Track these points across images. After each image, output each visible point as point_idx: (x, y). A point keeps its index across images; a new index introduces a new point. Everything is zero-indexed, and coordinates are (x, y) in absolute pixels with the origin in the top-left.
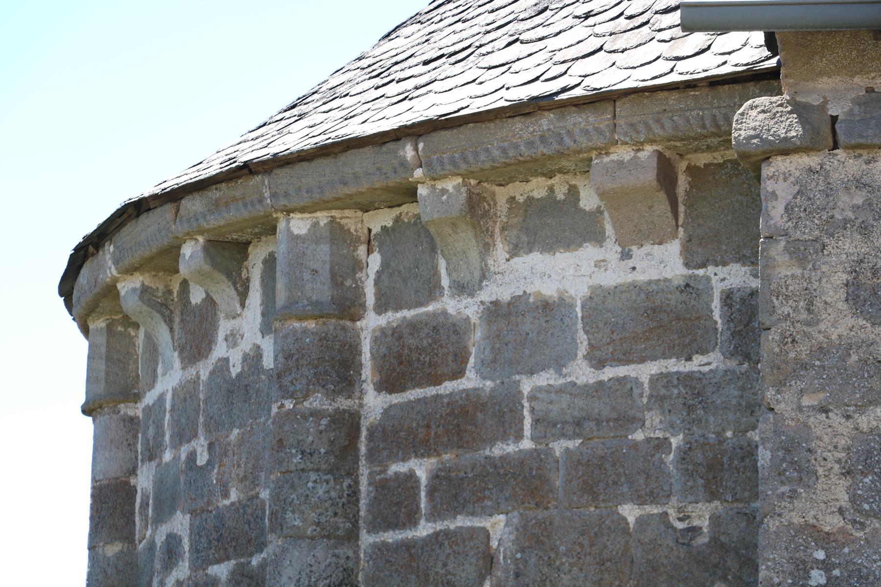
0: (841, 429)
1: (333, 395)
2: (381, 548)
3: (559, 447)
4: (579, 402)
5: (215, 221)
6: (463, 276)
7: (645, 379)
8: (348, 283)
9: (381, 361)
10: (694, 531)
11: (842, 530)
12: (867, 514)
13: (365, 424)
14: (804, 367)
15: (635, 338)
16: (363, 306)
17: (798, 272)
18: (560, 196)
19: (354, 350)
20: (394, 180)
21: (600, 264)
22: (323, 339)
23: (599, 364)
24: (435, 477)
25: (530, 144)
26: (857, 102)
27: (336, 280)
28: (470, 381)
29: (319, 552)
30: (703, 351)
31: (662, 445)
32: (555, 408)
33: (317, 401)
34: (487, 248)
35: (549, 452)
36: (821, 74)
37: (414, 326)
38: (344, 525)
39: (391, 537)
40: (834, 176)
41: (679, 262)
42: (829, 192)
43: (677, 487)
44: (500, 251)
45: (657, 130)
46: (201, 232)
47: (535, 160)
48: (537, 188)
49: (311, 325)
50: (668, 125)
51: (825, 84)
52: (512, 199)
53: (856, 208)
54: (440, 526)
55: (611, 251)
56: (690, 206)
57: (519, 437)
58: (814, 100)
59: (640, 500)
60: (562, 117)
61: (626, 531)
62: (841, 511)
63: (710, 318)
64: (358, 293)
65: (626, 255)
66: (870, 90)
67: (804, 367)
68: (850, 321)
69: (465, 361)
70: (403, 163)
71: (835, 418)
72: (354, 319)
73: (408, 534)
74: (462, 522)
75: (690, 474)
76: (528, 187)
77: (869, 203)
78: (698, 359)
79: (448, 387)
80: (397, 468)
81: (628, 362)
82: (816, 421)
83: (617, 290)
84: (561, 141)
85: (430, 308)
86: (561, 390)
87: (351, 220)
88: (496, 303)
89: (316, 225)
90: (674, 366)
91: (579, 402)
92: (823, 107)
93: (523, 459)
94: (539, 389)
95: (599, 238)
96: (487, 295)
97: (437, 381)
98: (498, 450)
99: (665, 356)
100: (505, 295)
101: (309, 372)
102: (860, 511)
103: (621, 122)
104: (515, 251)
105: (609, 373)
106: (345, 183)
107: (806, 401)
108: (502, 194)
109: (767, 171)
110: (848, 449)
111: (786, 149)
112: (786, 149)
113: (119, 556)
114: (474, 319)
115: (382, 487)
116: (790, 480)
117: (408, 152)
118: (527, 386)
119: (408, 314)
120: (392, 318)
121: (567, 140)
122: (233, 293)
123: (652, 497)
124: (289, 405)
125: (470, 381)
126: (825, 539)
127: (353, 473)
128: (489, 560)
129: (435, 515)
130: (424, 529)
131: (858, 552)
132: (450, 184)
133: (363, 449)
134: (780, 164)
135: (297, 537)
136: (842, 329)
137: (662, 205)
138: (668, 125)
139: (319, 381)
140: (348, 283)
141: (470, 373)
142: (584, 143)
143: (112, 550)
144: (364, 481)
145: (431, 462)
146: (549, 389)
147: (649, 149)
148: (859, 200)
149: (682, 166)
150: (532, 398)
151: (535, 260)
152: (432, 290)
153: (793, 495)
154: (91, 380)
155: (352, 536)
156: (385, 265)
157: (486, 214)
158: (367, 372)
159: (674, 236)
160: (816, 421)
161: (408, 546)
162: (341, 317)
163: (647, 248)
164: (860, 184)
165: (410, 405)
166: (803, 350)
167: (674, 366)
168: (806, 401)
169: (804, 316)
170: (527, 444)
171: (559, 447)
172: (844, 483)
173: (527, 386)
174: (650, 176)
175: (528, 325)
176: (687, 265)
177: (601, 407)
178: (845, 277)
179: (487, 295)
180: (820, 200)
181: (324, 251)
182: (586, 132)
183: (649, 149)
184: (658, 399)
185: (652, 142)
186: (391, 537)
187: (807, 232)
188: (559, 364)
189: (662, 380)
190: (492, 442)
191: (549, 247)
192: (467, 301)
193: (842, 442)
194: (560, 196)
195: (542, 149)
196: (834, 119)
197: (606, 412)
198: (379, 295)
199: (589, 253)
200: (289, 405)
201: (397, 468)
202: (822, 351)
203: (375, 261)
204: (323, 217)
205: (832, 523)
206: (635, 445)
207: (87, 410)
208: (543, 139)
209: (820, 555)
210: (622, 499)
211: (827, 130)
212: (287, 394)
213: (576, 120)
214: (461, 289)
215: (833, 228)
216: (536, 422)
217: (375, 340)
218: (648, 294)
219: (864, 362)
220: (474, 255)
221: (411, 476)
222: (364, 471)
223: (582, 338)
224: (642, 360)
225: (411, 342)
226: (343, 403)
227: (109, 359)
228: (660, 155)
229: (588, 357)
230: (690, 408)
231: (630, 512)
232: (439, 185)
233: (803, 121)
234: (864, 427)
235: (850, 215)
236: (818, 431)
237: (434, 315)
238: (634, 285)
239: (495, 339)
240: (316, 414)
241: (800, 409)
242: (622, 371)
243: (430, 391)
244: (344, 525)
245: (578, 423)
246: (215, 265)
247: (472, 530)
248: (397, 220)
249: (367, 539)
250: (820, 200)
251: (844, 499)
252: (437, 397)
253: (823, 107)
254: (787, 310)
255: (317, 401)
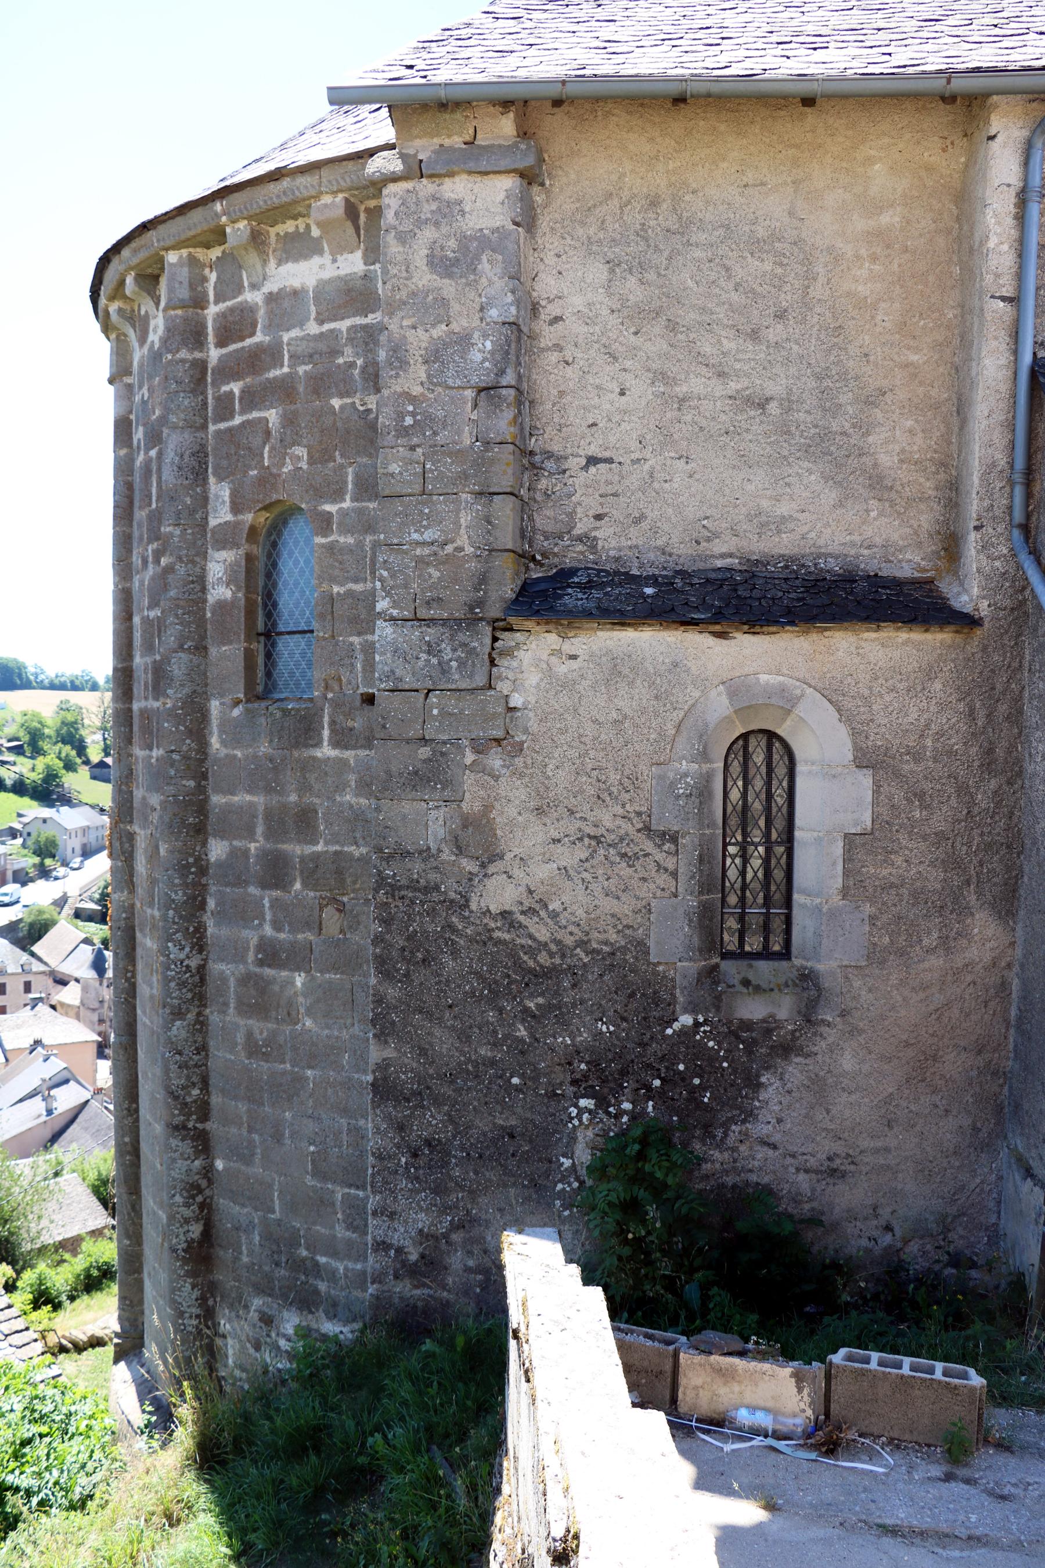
0: (423, 338)
1: (191, 350)
2: (218, 432)
3: (301, 370)
4: (312, 345)
5: (135, 261)
6: (254, 279)
7: (344, 329)
8: (199, 289)
9: (217, 331)
10: (369, 411)
11: (422, 394)
12: (435, 385)
13: (210, 366)
14: (404, 303)
15: (339, 307)
16: (208, 302)
17: (401, 249)
18: (302, 230)
19: (204, 327)
20: (213, 224)
21: (322, 267)
22: (186, 320)
23: (321, 322)
24: (243, 391)
25: (278, 196)
26: (434, 152)
27: (192, 287)
28: (259, 337)
29: (186, 436)
30: (373, 312)
31: (352, 365)
32: (300, 349)
33: (183, 354)
34: (265, 262)
35: (297, 373)
36: (416, 137)
37: (232, 310)
38: (199, 421)
39: (223, 426)
40: (421, 194)
41: (361, 262)
42: (417, 203)
43: (360, 387)
44: (272, 263)
45: (343, 183)
46: (132, 269)
47: (282, 206)
48: (289, 226)
49: (179, 312)
50: (348, 180)
51: (418, 143)
52: (278, 234)
53: (433, 212)
54: (245, 418)
55: (327, 258)
56: (366, 231)
57: (282, 366)
58: (411, 152)
59: (341, 396)
60: (294, 180)
61: (334, 413)
62: (422, 383)
63: (377, 293)
64: (205, 294)
65: (334, 261)
66: (441, 146)
67: (404, 303)
68: (429, 277)
69: (256, 327)
70: (216, 214)
71: (420, 332)
72: (203, 308)
73: (230, 424)
74: (255, 414)
75: (366, 380)
76: (285, 226)
77: (439, 209)
78: (371, 316)
79: (248, 342)
80: (225, 388)
81: (336, 320)
82: (410, 334)
83: (330, 281)
84: (293, 194)
85: (239, 299)
86: (302, 339)
87: (200, 253)
88: (270, 293)
89: (181, 257)
90: (359, 321)
91: (312, 345)
92: (415, 155)
93: (284, 378)
94: (292, 339)
95: (320, 252)
96: (266, 289)
97: (242, 339)
98: (274, 373)
99: (354, 316)
100: (275, 290)
101: (178, 338)
102: (432, 383)
103: (324, 180)
104: (279, 264)
105: (327, 327)
106: (190, 229)
107: (405, 323)
108: (273, 231)
109: (385, 192)
110: (426, 349)
111: (395, 179)
112: (395, 179)
113: (126, 455)
114: (260, 303)
115: (218, 399)
116: (396, 368)
117: (218, 207)
118: (286, 337)
119: (229, 303)
120: (222, 306)
121: (297, 193)
122: (152, 303)
123: (347, 394)
124: (170, 357)
125: (259, 337)
126: (413, 399)
127: (204, 393)
128: (268, 433)
129: (243, 412)
130: (238, 420)
131: (430, 406)
132: (242, 225)
133: (209, 380)
134: (392, 188)
135: (175, 427)
136: (424, 282)
137: (351, 230)
138: (348, 180)
139: (184, 343)
140: (199, 289)
141: (259, 333)
142: (305, 194)
143: (123, 452)
144: (210, 397)
145: (240, 384)
146: (296, 339)
147: (341, 196)
148: (434, 207)
149: (362, 208)
150: (288, 344)
151: (289, 267)
152: (239, 289)
153: (397, 376)
154: (111, 366)
155: (204, 427)
156: (218, 278)
157: (263, 243)
158: (211, 338)
159: (359, 247)
160: (410, 334)
161: (230, 430)
162: (195, 307)
163: (345, 256)
164: (434, 198)
165: (230, 354)
166: (403, 294)
167: (359, 321)
168: (405, 323)
169: (404, 274)
170: (286, 370)
171: (301, 370)
172: (424, 368)
173: (286, 337)
174: (340, 211)
175: (286, 304)
176: (365, 264)
177: (322, 346)
178: (426, 252)
179: (266, 289)
180: (413, 208)
181: (185, 271)
182: (306, 187)
183: (341, 196)
184: (351, 340)
185: (341, 191)
186: (223, 426)
187: (406, 226)
188: (301, 324)
189: (352, 329)
190: (269, 370)
191: (296, 260)
192: (257, 293)
193: (424, 345)
194: (302, 230)
195: (284, 199)
196: (421, 161)
197: (325, 349)
198: (216, 295)
199: (316, 260)
200: (170, 357)
201: (225, 388)
202: (414, 294)
203: (213, 277)
204: (184, 252)
205: (417, 390)
206: (339, 366)
207: (111, 381)
208: (284, 193)
209: (411, 408)
210: (332, 396)
211: (417, 167)
212: (169, 351)
213: (302, 180)
214: (254, 287)
215: (420, 223)
216: (291, 357)
217: (214, 320)
218: (346, 282)
219: (435, 299)
220: (259, 267)
221: (231, 392)
222: (210, 392)
223: (313, 308)
224: (343, 319)
225: (231, 319)
226: (198, 355)
227: (118, 354)
228: (347, 200)
229: (316, 319)
230: (367, 344)
231: (336, 403)
232: (237, 226)
233: (404, 162)
234: (435, 336)
235: (429, 216)
236: (411, 339)
237: (241, 303)
238: (339, 277)
239: (270, 313)
240: (183, 361)
241: (402, 327)
242: (332, 325)
243: (240, 345)
244: (199, 421)
245: (311, 356)
246: (141, 287)
247: (260, 419)
248: (224, 252)
249: (212, 428)
250: (413, 208)
251: (423, 376)
252: (243, 348)
253: (415, 155)
254: (395, 271)
255: (183, 354)
